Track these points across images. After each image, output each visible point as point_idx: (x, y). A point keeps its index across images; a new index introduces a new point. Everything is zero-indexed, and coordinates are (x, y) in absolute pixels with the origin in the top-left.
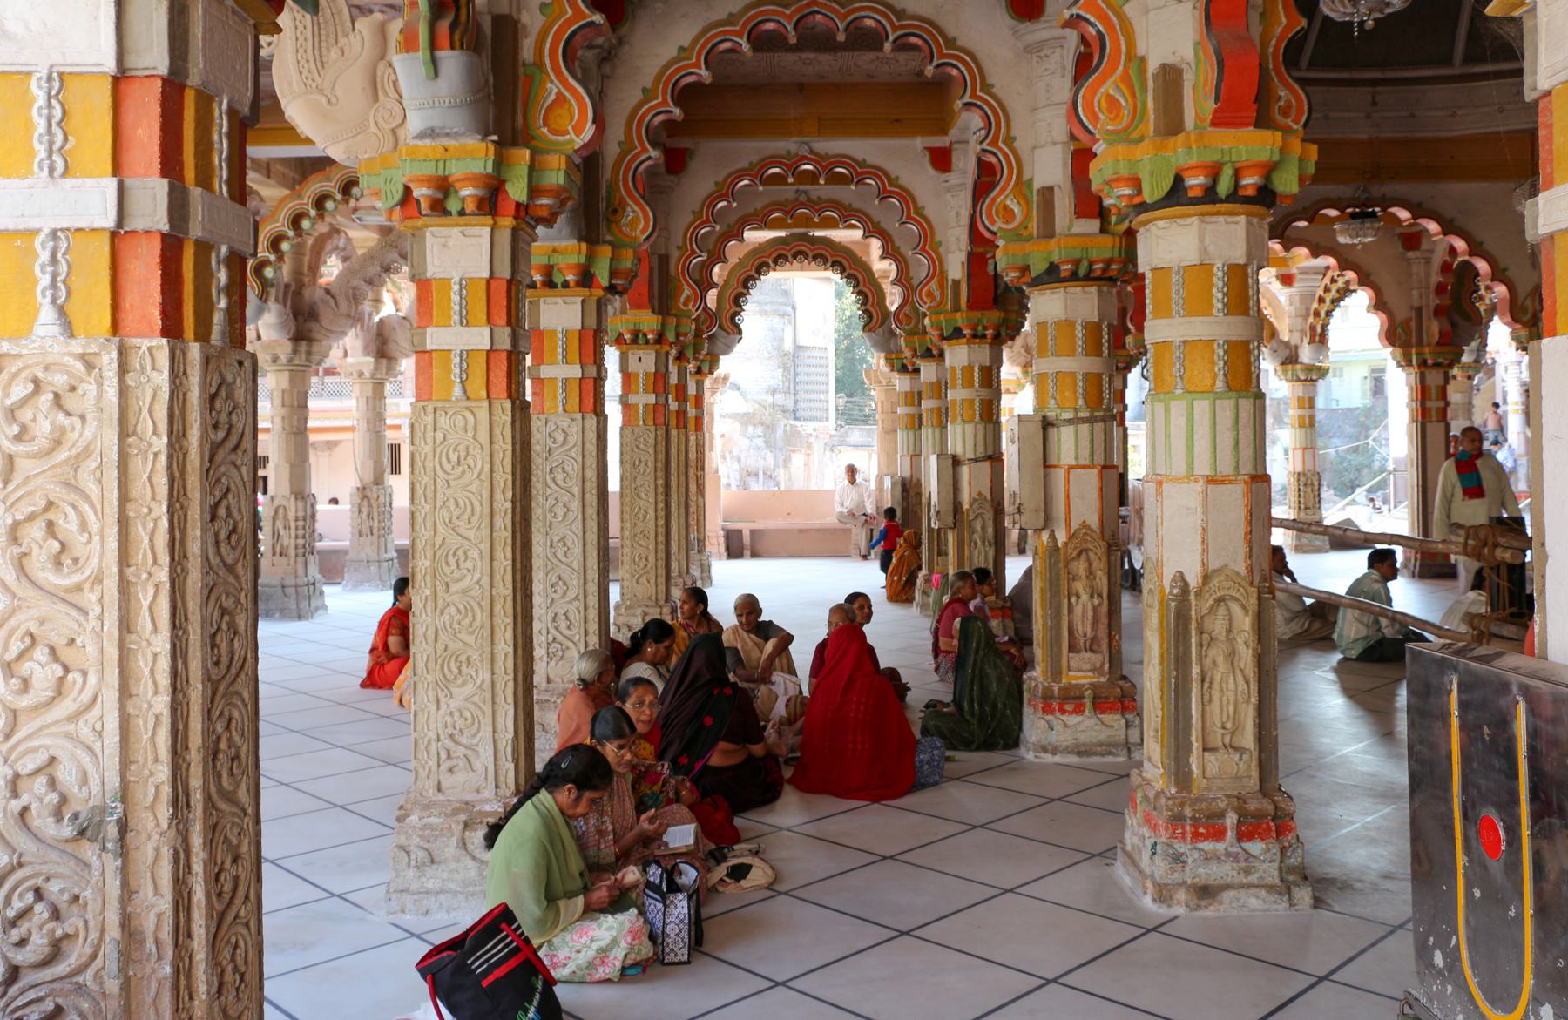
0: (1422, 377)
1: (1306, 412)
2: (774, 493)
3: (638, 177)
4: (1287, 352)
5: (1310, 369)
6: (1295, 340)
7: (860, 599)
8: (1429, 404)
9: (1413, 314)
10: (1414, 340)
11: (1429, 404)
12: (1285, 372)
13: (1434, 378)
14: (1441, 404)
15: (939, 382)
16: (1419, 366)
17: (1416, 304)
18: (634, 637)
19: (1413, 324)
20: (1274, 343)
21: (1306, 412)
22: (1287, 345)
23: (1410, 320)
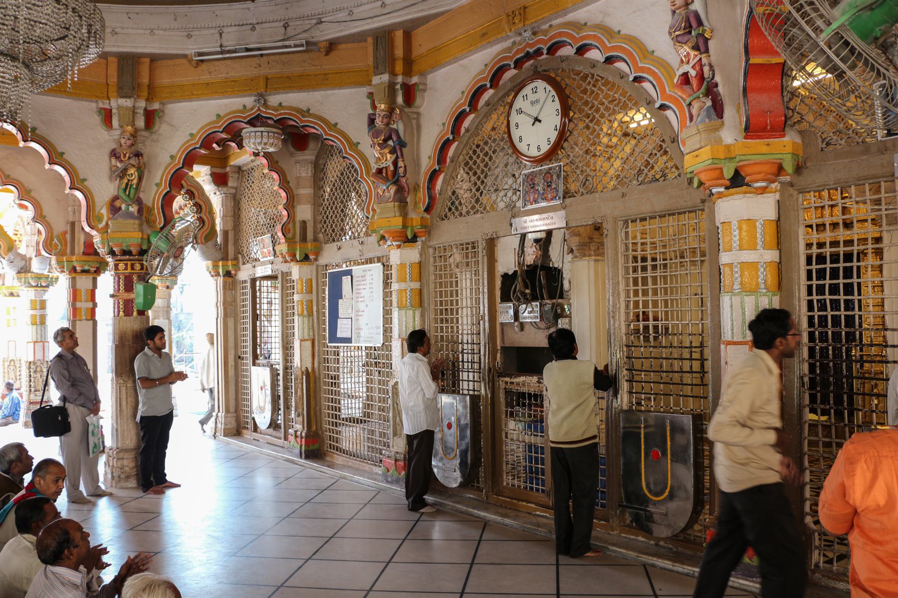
0: (73, 282)
1: (38, 313)
2: (789, 330)
3: (236, 124)
4: (23, 263)
5: (39, 277)
6: (31, 253)
7: (53, 469)
8: (78, 305)
9: (69, 228)
10: (68, 251)
11: (78, 305)
12: (19, 279)
13: (84, 282)
14: (90, 305)
15: (420, 263)
16: (70, 272)
17: (71, 219)
18: (781, 445)
19: (68, 236)
20: (11, 256)
21: (38, 313)
22: (23, 257)
23: (66, 233)
